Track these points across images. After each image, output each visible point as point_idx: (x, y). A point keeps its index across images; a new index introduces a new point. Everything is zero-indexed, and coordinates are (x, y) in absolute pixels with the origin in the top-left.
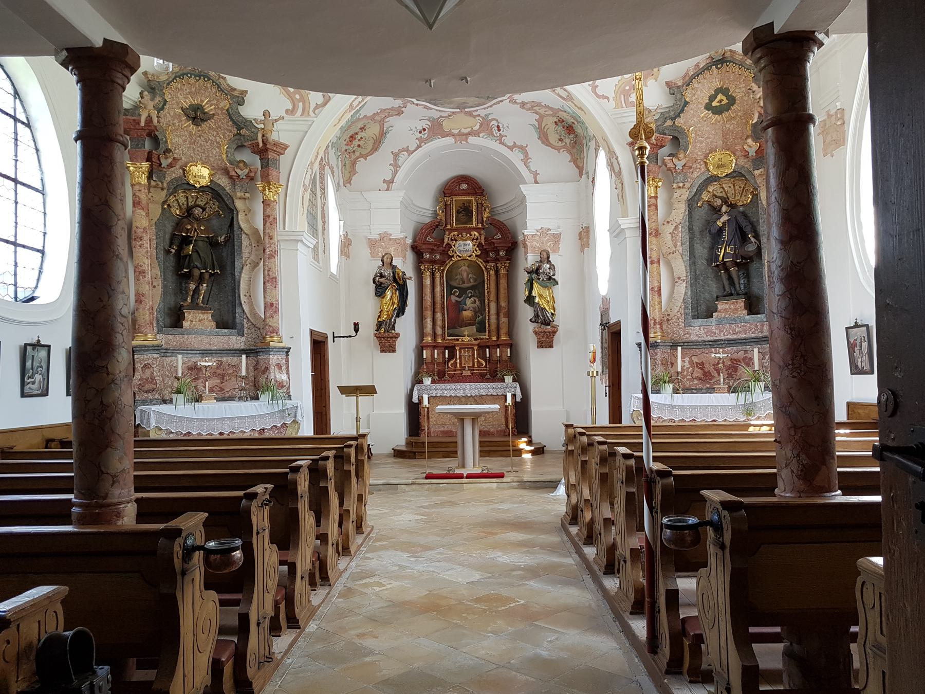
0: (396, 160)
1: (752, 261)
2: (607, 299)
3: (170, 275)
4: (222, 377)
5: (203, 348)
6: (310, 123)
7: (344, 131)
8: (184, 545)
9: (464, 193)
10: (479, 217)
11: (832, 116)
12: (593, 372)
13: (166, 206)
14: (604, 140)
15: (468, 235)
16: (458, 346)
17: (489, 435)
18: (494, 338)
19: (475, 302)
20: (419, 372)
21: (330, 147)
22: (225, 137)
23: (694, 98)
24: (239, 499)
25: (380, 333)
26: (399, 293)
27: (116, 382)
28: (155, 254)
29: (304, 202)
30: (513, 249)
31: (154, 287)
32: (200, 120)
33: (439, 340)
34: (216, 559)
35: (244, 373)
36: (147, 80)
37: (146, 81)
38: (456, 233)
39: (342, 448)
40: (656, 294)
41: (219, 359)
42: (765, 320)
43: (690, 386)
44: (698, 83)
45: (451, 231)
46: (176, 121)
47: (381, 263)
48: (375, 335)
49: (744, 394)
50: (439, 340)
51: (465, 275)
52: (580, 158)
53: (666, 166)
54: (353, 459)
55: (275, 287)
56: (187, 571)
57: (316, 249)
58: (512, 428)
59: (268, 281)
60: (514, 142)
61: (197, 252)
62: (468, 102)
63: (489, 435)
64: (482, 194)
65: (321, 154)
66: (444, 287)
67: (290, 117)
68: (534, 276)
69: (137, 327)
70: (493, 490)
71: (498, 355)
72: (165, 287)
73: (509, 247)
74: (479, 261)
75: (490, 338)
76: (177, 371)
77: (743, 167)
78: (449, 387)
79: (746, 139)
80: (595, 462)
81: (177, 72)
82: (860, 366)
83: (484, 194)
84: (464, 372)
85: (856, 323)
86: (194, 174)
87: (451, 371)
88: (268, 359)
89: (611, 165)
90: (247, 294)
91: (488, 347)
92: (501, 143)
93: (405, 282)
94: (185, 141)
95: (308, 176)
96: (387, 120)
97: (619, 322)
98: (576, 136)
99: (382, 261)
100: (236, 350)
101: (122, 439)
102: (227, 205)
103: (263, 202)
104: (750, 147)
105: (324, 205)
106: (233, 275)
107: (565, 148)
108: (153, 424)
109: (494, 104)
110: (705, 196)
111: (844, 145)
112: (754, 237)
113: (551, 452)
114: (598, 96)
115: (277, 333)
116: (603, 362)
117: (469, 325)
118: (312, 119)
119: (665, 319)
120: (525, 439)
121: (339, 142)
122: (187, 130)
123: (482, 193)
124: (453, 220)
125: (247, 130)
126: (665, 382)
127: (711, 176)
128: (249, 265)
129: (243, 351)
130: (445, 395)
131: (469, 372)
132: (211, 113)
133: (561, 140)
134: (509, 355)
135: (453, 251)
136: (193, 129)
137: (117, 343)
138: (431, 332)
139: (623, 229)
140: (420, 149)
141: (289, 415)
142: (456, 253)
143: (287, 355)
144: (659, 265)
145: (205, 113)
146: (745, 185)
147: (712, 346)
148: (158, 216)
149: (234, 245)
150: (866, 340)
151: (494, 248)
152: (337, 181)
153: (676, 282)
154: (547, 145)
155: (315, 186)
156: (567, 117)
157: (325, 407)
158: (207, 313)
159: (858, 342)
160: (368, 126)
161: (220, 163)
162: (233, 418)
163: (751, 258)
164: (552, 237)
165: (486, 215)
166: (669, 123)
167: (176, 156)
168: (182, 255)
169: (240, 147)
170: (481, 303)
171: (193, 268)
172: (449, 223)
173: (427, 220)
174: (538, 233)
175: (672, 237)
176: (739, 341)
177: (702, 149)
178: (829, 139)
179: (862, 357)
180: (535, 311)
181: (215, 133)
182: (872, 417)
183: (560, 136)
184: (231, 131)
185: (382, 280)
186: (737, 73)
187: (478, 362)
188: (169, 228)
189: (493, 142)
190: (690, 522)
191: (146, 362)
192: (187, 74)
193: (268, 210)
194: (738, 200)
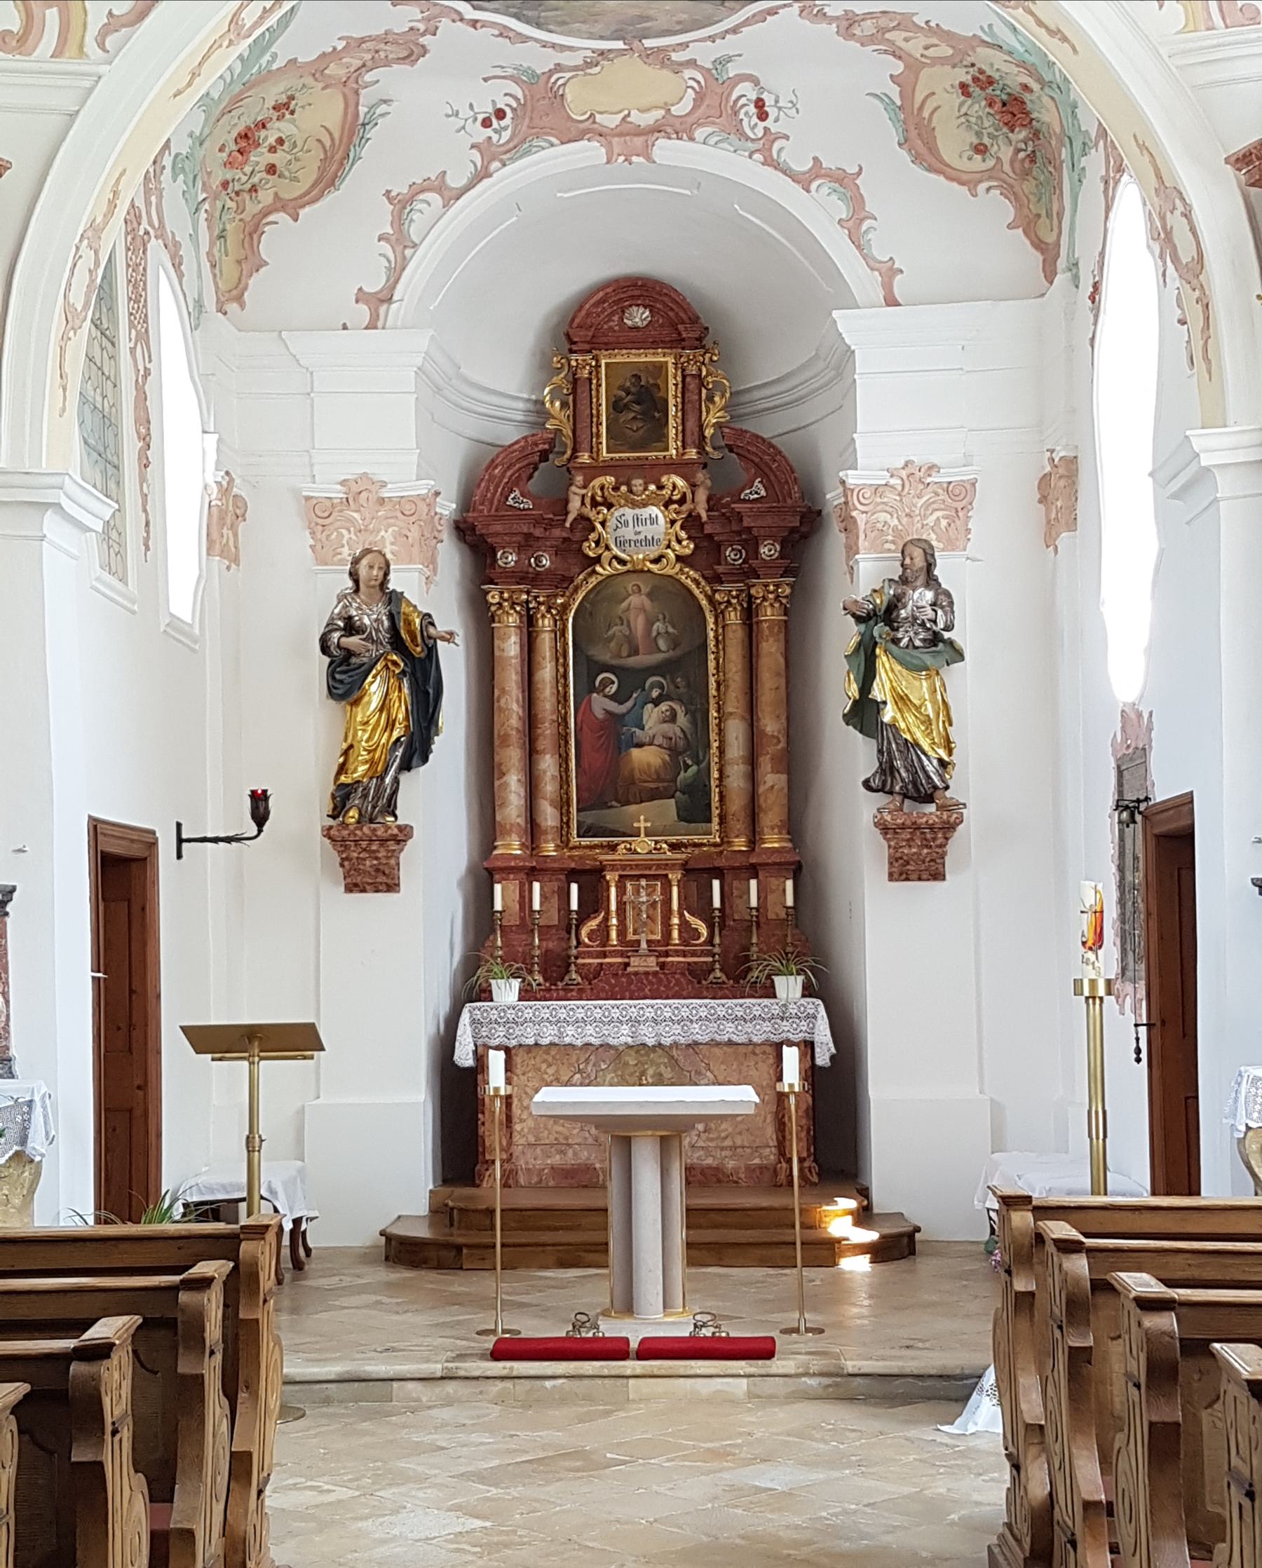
0: (399, 221)
2: (1140, 715)
6: (87, 84)
7: (217, 113)
9: (637, 339)
10: (691, 424)
12: (1093, 983)
14: (1142, 147)
15: (652, 487)
16: (613, 868)
17: (719, 1181)
18: (740, 844)
19: (673, 718)
20: (479, 958)
21: (168, 171)
25: (344, 825)
26: (411, 688)
29: (67, 369)
30: (805, 536)
33: (550, 849)
38: (611, 479)
39: (174, 1289)
45: (593, 471)
47: (350, 584)
48: (327, 831)
50: (550, 849)
51: (639, 624)
52: (1049, 215)
54: (213, 1331)
57: (114, 535)
58: (801, 1160)
60: (816, 159)
62: (651, 12)
63: (719, 1181)
64: (699, 343)
65: (132, 190)
66: (565, 665)
68: (879, 630)
70: (732, 1402)
71: (754, 902)
73: (793, 530)
74: (689, 577)
75: (725, 841)
78: (580, 1014)
80: (1128, 1375)
83: (708, 341)
84: (634, 961)
87: (590, 955)
89: (1163, 239)
91: (718, 873)
92: (769, 162)
93: (432, 652)
95: (81, 278)
96: (368, 77)
97: (1186, 803)
98: (1036, 134)
99: (354, 576)
107: (990, 178)
109: (746, 23)
113: (941, 1249)
116: (1124, 937)
117: (654, 795)
118: (93, 69)
120: (851, 1204)
121: (200, 153)
123: (700, 339)
124: (598, 435)
130: (567, 1040)
131: (652, 961)
133: (980, 149)
134: (790, 902)
135: (597, 543)
138: (521, 821)
139: (1207, 469)
140: (486, 182)
142: (607, 548)
151: (739, 533)
154: (930, 169)
155: (112, 309)
156: (1005, 68)
160: (300, 100)
164: (943, 496)
165: (712, 418)
170: (694, 722)
172: (586, 445)
173: (510, 434)
174: (895, 482)
180: (880, 751)
183: (979, 134)
185: (353, 641)
187: (684, 924)
189: (742, 159)
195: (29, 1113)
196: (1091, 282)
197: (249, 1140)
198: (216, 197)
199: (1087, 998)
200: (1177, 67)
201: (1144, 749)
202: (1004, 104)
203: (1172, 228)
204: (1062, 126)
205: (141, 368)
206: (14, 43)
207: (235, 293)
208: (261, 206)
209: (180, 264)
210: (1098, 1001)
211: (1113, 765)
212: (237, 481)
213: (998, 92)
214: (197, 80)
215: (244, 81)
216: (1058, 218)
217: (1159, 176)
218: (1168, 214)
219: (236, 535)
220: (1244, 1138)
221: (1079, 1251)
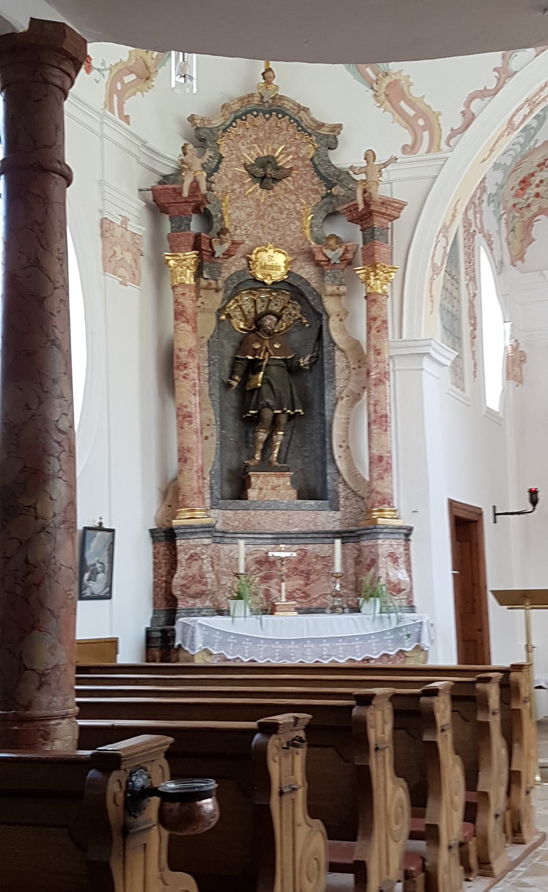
3: (231, 421)
4: (307, 575)
5: (277, 530)
6: (442, 163)
8: (127, 785)
13: (223, 317)
21: (485, 203)
22: (308, 203)
24: (252, 732)
27: (48, 529)
28: (207, 388)
29: (434, 293)
31: (206, 438)
32: (271, 181)
34: (171, 810)
35: (338, 568)
36: (195, 127)
37: (193, 129)
41: (302, 547)
46: (236, 186)
55: (386, 430)
56: (131, 828)
59: (375, 421)
61: (269, 382)
67: (410, 158)
69: (181, 498)
72: (222, 438)
76: (237, 566)
81: (238, 111)
86: (263, 264)
88: (376, 546)
90: (344, 444)
94: (250, 215)
95: (440, 252)
100: (327, 532)
101: (57, 617)
102: (312, 308)
103: (366, 297)
105: (474, 297)
106: (323, 415)
108: (199, 645)
115: (389, 504)
121: (502, 191)
122: (252, 198)
125: (342, 186)
128: (346, 399)
129: (337, 534)
132: (288, 167)
136: (261, 194)
137: (51, 472)
141: (408, 636)
143: (407, 540)
145: (278, 169)
148: (211, 332)
149: (323, 369)
152: (498, 259)
155: (457, 267)
157: (480, 630)
158: (284, 476)
161: (301, 242)
162: (320, 640)
167: (236, 238)
168: (248, 389)
169: (332, 215)
171: (264, 407)
181: (293, 198)
184: (317, 192)
188: (229, 349)
191: (192, 551)
192: (251, 112)
193: (374, 309)
195: (420, 628)
197: (527, 646)
198: (509, 212)
205: (471, 292)
206: (409, 150)
207: (520, 256)
208: (532, 213)
209: (492, 244)
212: (522, 344)
214: (493, 153)
215: (522, 154)
219: (521, 370)
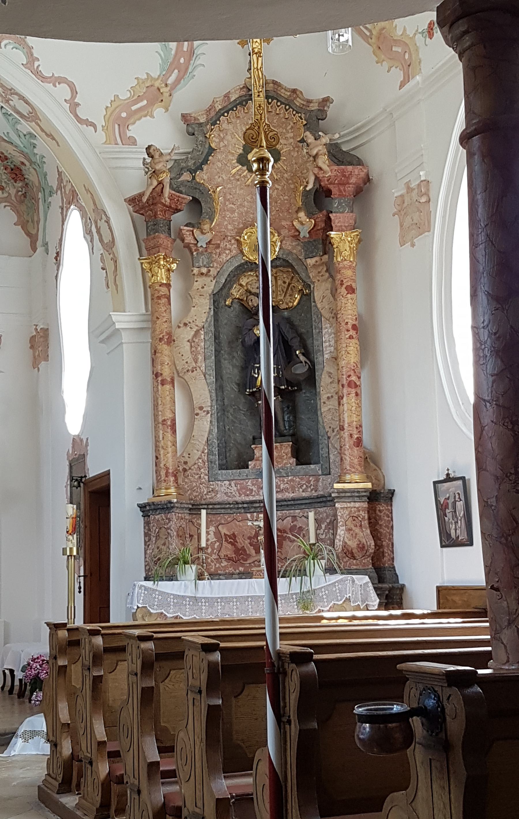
1: (300, 390)
2: (81, 440)
11: (413, 189)
12: (71, 549)
14: (88, 191)
23: (222, 144)
40: (169, 430)
42: (320, 472)
43: (217, 569)
44: (229, 123)
49: (299, 578)
52: (33, 221)
53: (183, 240)
77: (290, 253)
79: (297, 212)
82: (453, 535)
85: (448, 475)
97: (107, 474)
98: (27, 184)
104: (302, 223)
107: (5, 202)
110: (236, 292)
111: (429, 231)
112: (303, 354)
114: (80, 120)
119: (181, 468)
126: (186, 563)
127: (246, 262)
139: (118, 330)
144: (174, 387)
146: (292, 279)
147: (247, 510)
150: (463, 498)
153: (197, 414)
159: (450, 502)
163: (299, 384)
166: (186, 177)
175: (191, 347)
176: (285, 503)
177: (233, 221)
178: (408, 221)
179: (456, 523)
182: (472, 606)
186: (282, 115)
190: (395, 709)
194: (281, 300)
196: (55, 251)
199: (68, 556)
200: (103, 158)
201: (84, 455)
202: (12, 170)
203: (100, 227)
204: (39, 183)
210: (73, 558)
211: (68, 463)
213: (9, 164)
216: (37, 223)
217: (95, 204)
218: (99, 221)
220: (136, 612)
221: (98, 634)
